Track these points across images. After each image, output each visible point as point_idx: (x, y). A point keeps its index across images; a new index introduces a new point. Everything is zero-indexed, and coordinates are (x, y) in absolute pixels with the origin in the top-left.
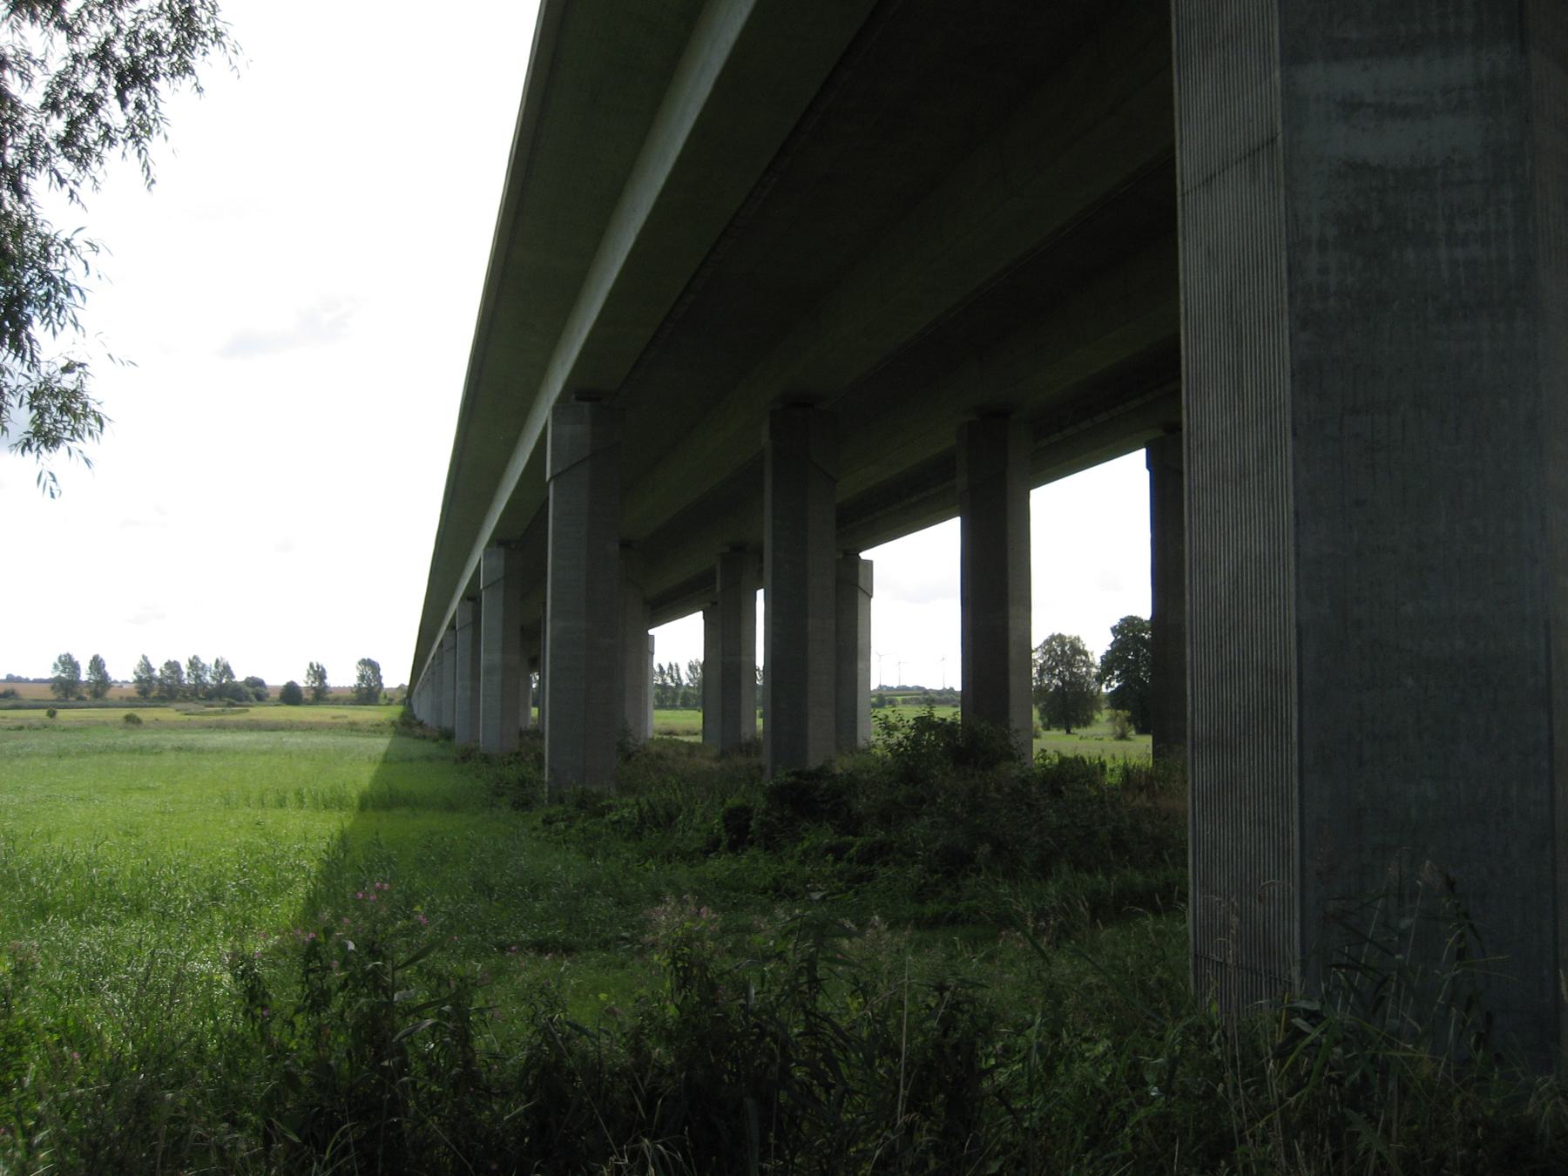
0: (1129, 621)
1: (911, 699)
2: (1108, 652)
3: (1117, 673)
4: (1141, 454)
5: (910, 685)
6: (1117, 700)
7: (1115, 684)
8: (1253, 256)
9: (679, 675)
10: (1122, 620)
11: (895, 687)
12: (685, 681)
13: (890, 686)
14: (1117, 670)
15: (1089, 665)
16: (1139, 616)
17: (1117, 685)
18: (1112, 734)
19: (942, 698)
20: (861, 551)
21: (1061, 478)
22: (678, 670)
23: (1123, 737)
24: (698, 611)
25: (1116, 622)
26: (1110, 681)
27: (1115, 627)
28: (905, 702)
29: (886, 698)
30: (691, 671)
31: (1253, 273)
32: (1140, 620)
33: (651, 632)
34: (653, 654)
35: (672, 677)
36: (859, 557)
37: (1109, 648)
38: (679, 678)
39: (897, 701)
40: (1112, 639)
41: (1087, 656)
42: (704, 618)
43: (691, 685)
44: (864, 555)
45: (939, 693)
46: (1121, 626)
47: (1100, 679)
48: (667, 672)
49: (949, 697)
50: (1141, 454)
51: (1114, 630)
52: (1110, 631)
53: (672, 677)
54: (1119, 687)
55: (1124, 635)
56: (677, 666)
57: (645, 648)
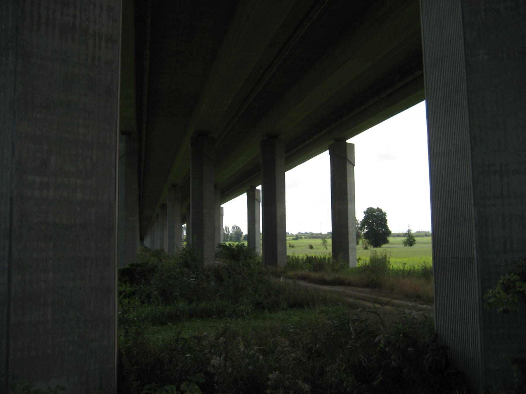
0: (370, 209)
1: (307, 237)
2: (363, 220)
3: (366, 226)
4: (328, 152)
5: (309, 232)
6: (367, 236)
7: (366, 230)
8: (453, 306)
9: (229, 230)
10: (367, 209)
11: (304, 233)
12: (231, 232)
13: (302, 232)
14: (366, 225)
15: (358, 224)
16: (373, 207)
17: (366, 231)
18: (363, 248)
19: (318, 236)
20: (346, 140)
21: (226, 202)
22: (228, 228)
23: (366, 248)
24: (245, 193)
25: (365, 210)
26: (364, 229)
27: (365, 211)
28: (305, 238)
29: (299, 237)
30: (233, 229)
31: (463, 331)
32: (373, 209)
33: (222, 206)
34: (223, 215)
35: (226, 231)
36: (256, 189)
37: (363, 218)
38: (229, 231)
39: (302, 237)
40: (364, 215)
41: (357, 221)
42: (247, 195)
43: (233, 233)
44: (349, 141)
45: (317, 234)
46: (367, 211)
47: (361, 229)
48: (225, 229)
49: (320, 236)
50: (328, 152)
51: (365, 213)
52: (363, 213)
53: (226, 231)
54: (367, 231)
55: (368, 214)
56: (228, 227)
57: (220, 214)
